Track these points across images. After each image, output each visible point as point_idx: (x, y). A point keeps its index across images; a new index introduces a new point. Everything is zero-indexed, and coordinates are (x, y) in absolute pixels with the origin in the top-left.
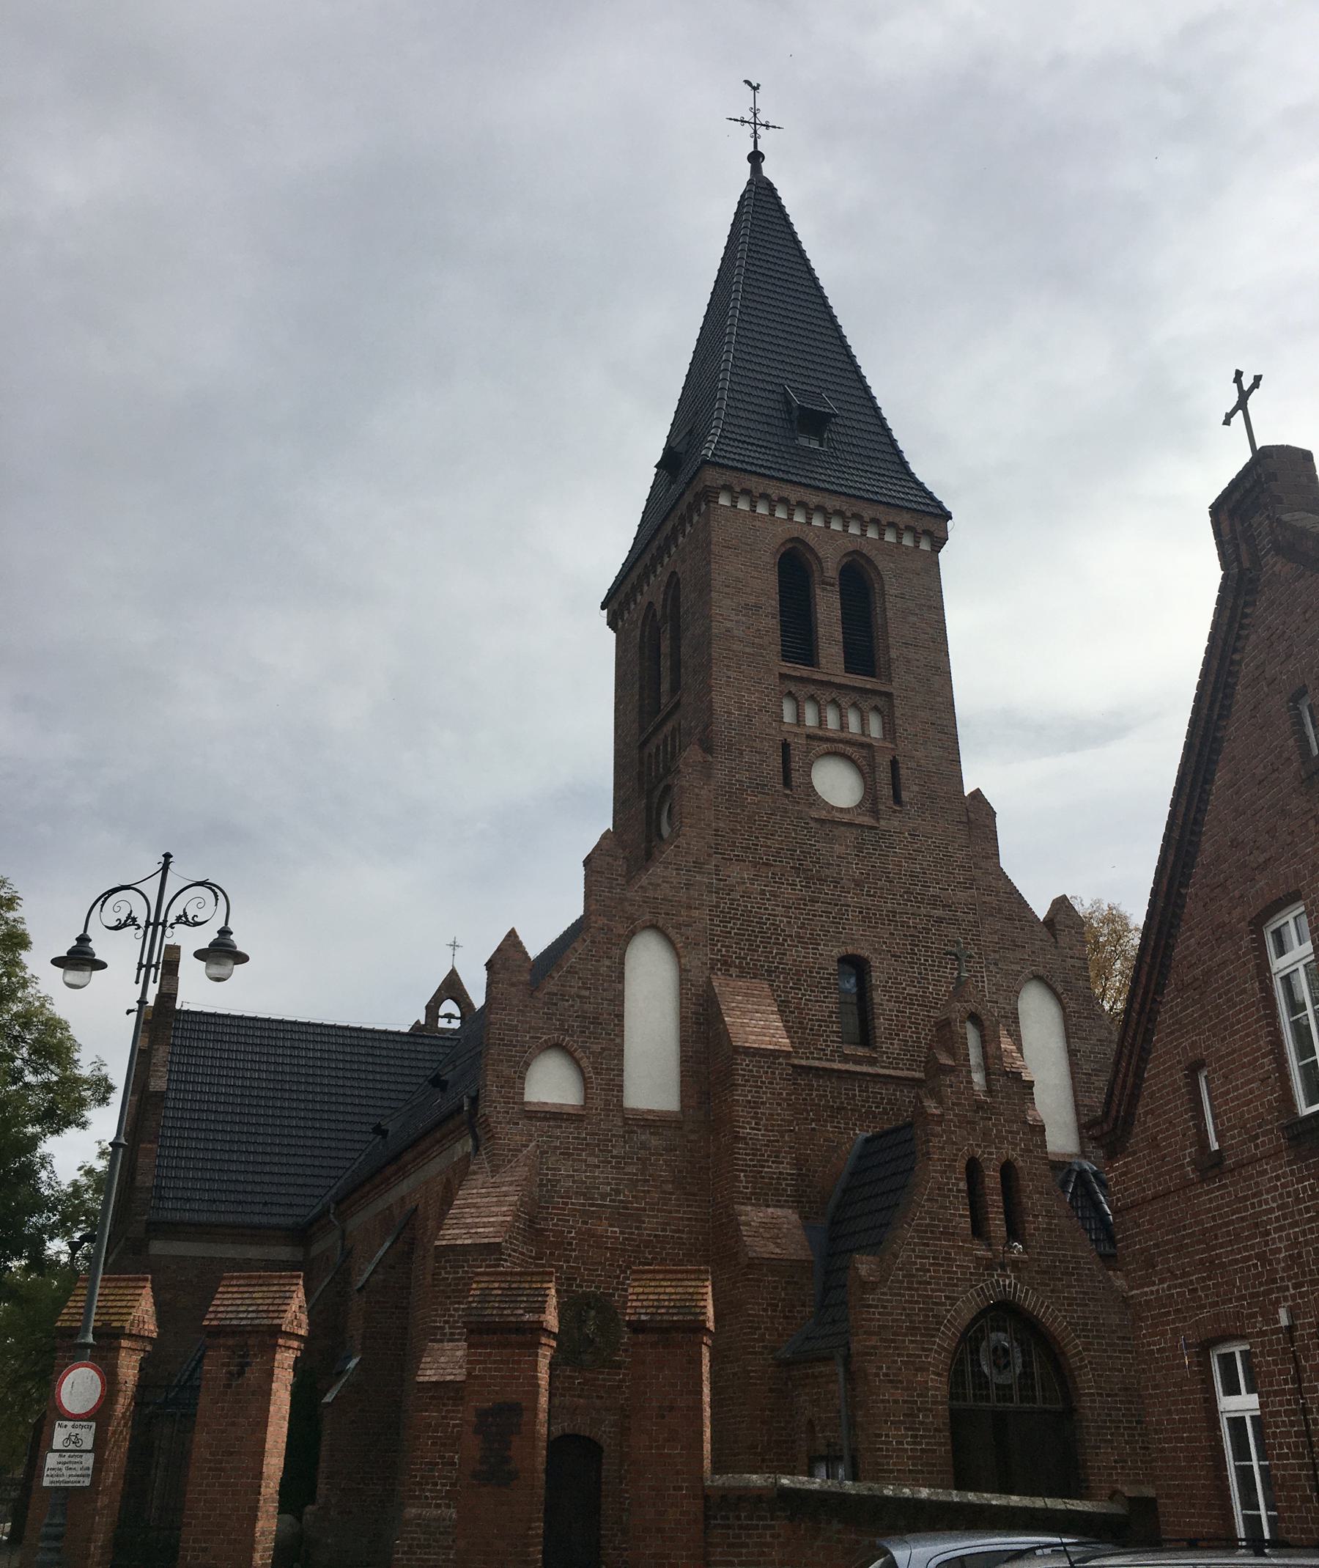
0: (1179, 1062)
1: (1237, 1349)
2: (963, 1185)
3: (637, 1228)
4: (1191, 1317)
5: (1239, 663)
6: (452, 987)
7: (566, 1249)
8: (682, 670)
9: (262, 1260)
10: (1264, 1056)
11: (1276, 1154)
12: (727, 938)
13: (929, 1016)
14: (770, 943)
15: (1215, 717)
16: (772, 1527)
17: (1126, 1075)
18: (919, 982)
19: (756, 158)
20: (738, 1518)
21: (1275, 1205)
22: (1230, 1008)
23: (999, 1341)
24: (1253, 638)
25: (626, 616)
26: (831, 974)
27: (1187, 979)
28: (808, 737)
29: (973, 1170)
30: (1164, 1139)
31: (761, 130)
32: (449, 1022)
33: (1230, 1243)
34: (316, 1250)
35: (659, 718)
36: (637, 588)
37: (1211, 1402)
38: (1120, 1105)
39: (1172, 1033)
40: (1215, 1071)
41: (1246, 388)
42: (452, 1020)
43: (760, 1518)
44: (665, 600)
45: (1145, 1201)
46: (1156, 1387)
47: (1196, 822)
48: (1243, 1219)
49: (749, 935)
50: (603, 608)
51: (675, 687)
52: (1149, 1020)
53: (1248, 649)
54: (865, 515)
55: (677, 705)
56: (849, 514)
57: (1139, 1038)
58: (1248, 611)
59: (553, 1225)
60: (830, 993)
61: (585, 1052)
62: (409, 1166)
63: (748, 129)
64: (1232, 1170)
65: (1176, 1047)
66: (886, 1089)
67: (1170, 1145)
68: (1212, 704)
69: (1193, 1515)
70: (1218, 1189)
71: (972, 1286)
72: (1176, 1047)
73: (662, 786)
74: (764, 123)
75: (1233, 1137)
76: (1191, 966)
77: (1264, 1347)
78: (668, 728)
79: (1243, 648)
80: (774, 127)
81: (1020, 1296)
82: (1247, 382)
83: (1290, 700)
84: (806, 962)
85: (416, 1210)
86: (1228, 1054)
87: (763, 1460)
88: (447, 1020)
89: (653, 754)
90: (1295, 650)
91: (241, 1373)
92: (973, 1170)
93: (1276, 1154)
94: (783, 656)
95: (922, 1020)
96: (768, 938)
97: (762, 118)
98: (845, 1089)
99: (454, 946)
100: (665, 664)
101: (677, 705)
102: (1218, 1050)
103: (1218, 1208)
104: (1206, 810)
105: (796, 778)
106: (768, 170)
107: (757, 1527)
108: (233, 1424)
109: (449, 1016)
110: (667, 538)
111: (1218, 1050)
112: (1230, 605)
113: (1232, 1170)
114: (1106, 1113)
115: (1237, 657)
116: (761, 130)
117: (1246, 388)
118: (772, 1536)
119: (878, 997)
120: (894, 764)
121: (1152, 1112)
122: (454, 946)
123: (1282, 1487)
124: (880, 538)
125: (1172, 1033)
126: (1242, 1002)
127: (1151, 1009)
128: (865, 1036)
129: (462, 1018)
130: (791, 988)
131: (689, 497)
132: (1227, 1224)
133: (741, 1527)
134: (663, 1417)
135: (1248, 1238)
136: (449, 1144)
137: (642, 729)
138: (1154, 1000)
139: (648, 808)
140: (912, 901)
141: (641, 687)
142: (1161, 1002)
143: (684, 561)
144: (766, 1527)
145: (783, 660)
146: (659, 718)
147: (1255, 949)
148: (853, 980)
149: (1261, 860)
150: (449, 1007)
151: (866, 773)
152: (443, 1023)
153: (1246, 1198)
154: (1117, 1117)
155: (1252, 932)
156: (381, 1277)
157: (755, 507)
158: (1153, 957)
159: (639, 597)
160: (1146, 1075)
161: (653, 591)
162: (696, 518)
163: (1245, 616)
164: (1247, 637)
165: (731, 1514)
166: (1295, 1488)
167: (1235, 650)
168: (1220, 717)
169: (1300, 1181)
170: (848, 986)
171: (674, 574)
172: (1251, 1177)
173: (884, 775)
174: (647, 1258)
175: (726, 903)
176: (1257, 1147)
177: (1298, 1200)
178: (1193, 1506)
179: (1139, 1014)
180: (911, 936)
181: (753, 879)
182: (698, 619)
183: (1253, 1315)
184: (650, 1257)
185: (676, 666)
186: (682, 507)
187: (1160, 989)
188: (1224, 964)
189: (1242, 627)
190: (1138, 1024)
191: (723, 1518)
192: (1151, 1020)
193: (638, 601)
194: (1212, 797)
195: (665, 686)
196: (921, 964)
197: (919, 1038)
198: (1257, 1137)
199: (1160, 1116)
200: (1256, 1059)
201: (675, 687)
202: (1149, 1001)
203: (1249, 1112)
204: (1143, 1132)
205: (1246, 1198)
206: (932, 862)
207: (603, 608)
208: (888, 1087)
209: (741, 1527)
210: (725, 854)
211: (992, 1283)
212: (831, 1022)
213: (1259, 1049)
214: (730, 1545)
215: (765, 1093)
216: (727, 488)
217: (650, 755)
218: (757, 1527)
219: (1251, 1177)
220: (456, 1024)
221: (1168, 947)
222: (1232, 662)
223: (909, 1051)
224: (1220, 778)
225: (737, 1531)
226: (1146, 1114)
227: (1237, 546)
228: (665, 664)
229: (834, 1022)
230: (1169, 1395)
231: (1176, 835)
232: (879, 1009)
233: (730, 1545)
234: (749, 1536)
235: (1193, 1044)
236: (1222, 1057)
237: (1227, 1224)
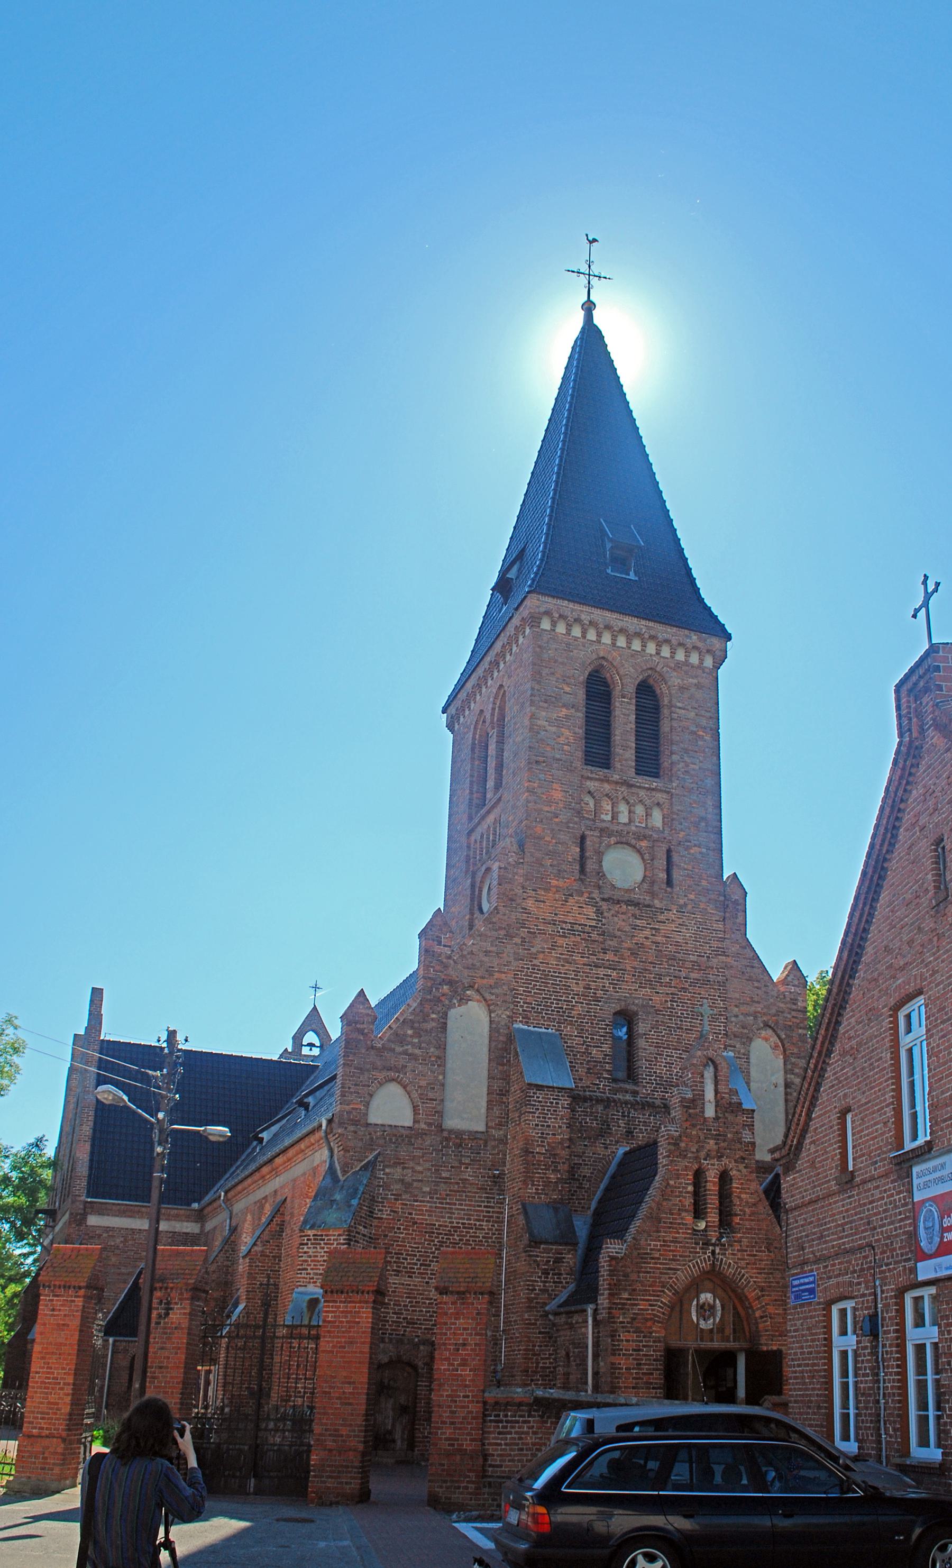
0: (835, 1107)
1: (849, 1305)
2: (690, 1188)
3: (449, 1218)
4: (822, 1284)
5: (904, 810)
6: (314, 1021)
7: (395, 1233)
8: (504, 772)
9: (170, 1232)
10: (887, 1106)
11: (886, 1175)
12: (528, 996)
13: (681, 1058)
14: (561, 1000)
15: (884, 852)
16: (529, 1422)
17: (800, 1115)
18: (675, 1031)
19: (589, 307)
20: (506, 1416)
21: (881, 1209)
22: (870, 1070)
23: (706, 1299)
24: (914, 792)
25: (462, 719)
26: (607, 1025)
27: (847, 1047)
28: (602, 830)
29: (699, 1175)
30: (820, 1162)
31: (594, 281)
32: (311, 1050)
33: (852, 1235)
34: (209, 1226)
35: (483, 811)
36: (471, 697)
37: (828, 1342)
38: (794, 1137)
39: (833, 1086)
40: (856, 1115)
41: (930, 590)
42: (313, 1048)
43: (521, 1416)
44: (493, 709)
45: (805, 1205)
46: (795, 1331)
47: (865, 930)
48: (862, 1219)
49: (545, 994)
50: (443, 712)
51: (498, 785)
52: (820, 1076)
53: (911, 800)
54: (660, 636)
55: (500, 799)
56: (646, 636)
57: (812, 1089)
58: (913, 770)
59: (387, 1215)
60: (606, 1040)
61: (415, 1086)
62: (281, 1168)
63: (583, 280)
64: (858, 1186)
65: (835, 1096)
66: (643, 1115)
67: (823, 1166)
68: (883, 841)
69: (808, 1413)
70: (849, 1197)
71: (690, 1261)
72: (835, 1096)
73: (483, 869)
74: (596, 274)
75: (862, 1162)
76: (850, 1038)
77: (863, 1304)
78: (490, 819)
79: (907, 800)
80: (605, 278)
81: (724, 1268)
82: (931, 588)
83: (932, 844)
84: (589, 1016)
85: (285, 1199)
86: (866, 1103)
87: (532, 1380)
88: (309, 1048)
89: (478, 841)
90: (940, 806)
91: (167, 1314)
92: (699, 1175)
93: (886, 1175)
94: (586, 760)
95: (676, 1061)
96: (560, 996)
97: (595, 270)
98: (612, 1115)
99: (316, 988)
100: (492, 764)
101: (500, 799)
102: (860, 1100)
103: (847, 1211)
104: (871, 922)
105: (590, 866)
106: (599, 319)
107: (518, 1422)
108: (162, 1348)
109: (311, 1045)
110: (497, 655)
111: (860, 1100)
112: (901, 765)
113: (858, 1186)
114: (784, 1143)
115: (902, 806)
116: (594, 281)
117: (930, 590)
118: (529, 1428)
119: (641, 1043)
120: (669, 851)
121: (813, 1142)
122: (316, 988)
123: (863, 1395)
124: (671, 656)
125: (833, 1086)
126: (878, 1066)
127: (822, 1068)
128: (632, 1075)
129: (321, 1047)
130: (576, 1036)
131: (516, 621)
132: (851, 1222)
133: (507, 1422)
134: (458, 1350)
135: (863, 1231)
136: (311, 1153)
137: (470, 818)
138: (824, 1062)
139: (473, 886)
140: (674, 966)
141: (471, 783)
142: (828, 1064)
143: (509, 677)
144: (524, 1422)
145: (586, 764)
146: (483, 811)
147: (891, 1029)
148: (625, 1030)
149: (902, 963)
150: (311, 1037)
151: (648, 860)
152: (305, 1051)
153: (865, 1204)
154: (791, 1146)
155: (891, 1016)
156: (260, 1249)
157: (570, 630)
158: (827, 1030)
159: (472, 705)
160: (813, 1116)
161: (484, 700)
162: (521, 640)
163: (910, 774)
164: (910, 791)
165: (501, 1414)
166: (870, 1395)
167: (902, 801)
168: (888, 851)
169: (899, 1193)
170: (620, 1034)
171: (501, 686)
172: (869, 1190)
173: (661, 863)
174: (455, 1239)
175: (529, 968)
176: (875, 1169)
177: (896, 1207)
178: (809, 1407)
179: (813, 1072)
180: (672, 994)
181: (551, 949)
182: (519, 728)
183: (859, 1284)
184: (458, 1238)
185: (500, 767)
186: (510, 630)
187: (829, 1052)
188: (871, 1038)
189: (908, 783)
190: (811, 1079)
191: (495, 1416)
192: (821, 1076)
193: (472, 708)
194: (876, 913)
195: (490, 784)
196: (678, 1017)
197: (672, 1075)
198: (876, 1162)
199: (819, 1145)
200: (882, 1108)
201: (498, 785)
202: (821, 1062)
203: (874, 1144)
204: (807, 1156)
205: (865, 1204)
206: (693, 934)
207: (443, 712)
208: (645, 1112)
209: (507, 1422)
210: (530, 928)
211: (705, 1258)
212: (604, 1063)
213: (885, 1100)
214: (499, 1433)
215: (550, 1118)
216: (548, 613)
217: (476, 841)
218: (518, 1422)
219: (869, 1190)
220: (316, 1052)
221: (838, 1023)
222: (899, 810)
223: (663, 1085)
224: (884, 897)
225: (505, 1424)
226: (811, 1143)
227: (910, 719)
228: (492, 764)
229: (608, 1063)
230: (803, 1336)
231: (849, 940)
232: (642, 1052)
233: (499, 1433)
234: (512, 1427)
235: (845, 1095)
236: (862, 1105)
237: (851, 1222)
